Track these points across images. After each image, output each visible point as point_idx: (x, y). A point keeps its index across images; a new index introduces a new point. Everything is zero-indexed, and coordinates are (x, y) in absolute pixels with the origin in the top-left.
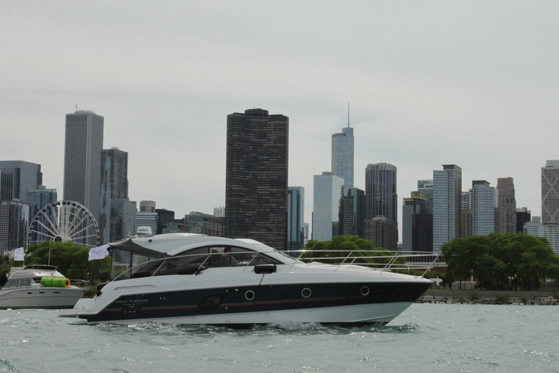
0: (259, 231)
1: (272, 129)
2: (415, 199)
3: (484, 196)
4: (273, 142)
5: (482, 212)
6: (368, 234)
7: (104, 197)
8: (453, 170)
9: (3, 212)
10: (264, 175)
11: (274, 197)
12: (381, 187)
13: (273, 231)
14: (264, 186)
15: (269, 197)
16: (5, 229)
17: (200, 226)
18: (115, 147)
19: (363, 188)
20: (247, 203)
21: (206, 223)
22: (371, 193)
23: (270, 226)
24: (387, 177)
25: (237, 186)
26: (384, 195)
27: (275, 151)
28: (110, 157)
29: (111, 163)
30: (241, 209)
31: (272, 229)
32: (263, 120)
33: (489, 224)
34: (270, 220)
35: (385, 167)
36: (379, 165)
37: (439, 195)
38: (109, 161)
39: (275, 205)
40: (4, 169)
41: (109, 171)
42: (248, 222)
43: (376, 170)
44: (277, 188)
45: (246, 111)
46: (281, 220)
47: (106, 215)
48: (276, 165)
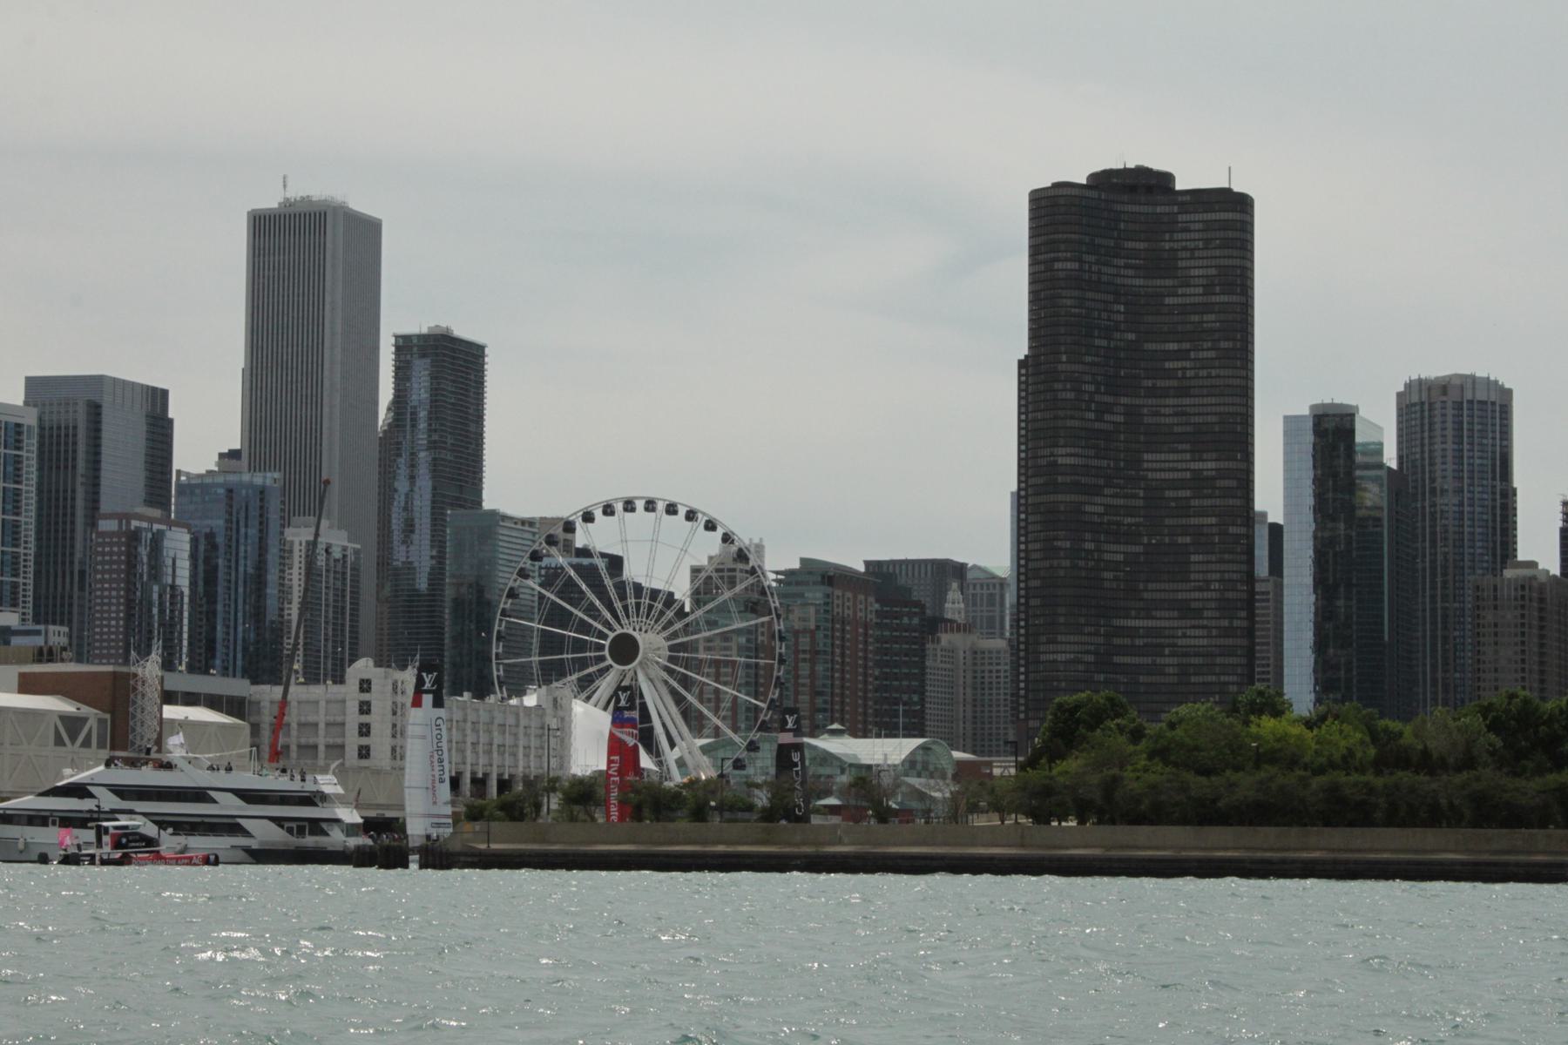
0: (1153, 618)
4: (1201, 290)
7: (407, 503)
9: (111, 556)
10: (1167, 411)
11: (1210, 491)
12: (1459, 458)
13: (1207, 618)
14: (1169, 452)
15: (1188, 493)
16: (110, 619)
17: (812, 604)
18: (444, 325)
19: (1394, 465)
23: (1195, 600)
24: (1480, 427)
25: (1072, 450)
26: (1469, 492)
27: (1207, 322)
28: (428, 361)
29: (432, 384)
30: (1088, 536)
31: (1203, 609)
32: (1159, 209)
35: (1474, 388)
38: (424, 375)
39: (1213, 520)
40: (44, 405)
42: (1114, 585)
43: (1444, 399)
45: (1093, 177)
46: (1235, 576)
47: (414, 568)
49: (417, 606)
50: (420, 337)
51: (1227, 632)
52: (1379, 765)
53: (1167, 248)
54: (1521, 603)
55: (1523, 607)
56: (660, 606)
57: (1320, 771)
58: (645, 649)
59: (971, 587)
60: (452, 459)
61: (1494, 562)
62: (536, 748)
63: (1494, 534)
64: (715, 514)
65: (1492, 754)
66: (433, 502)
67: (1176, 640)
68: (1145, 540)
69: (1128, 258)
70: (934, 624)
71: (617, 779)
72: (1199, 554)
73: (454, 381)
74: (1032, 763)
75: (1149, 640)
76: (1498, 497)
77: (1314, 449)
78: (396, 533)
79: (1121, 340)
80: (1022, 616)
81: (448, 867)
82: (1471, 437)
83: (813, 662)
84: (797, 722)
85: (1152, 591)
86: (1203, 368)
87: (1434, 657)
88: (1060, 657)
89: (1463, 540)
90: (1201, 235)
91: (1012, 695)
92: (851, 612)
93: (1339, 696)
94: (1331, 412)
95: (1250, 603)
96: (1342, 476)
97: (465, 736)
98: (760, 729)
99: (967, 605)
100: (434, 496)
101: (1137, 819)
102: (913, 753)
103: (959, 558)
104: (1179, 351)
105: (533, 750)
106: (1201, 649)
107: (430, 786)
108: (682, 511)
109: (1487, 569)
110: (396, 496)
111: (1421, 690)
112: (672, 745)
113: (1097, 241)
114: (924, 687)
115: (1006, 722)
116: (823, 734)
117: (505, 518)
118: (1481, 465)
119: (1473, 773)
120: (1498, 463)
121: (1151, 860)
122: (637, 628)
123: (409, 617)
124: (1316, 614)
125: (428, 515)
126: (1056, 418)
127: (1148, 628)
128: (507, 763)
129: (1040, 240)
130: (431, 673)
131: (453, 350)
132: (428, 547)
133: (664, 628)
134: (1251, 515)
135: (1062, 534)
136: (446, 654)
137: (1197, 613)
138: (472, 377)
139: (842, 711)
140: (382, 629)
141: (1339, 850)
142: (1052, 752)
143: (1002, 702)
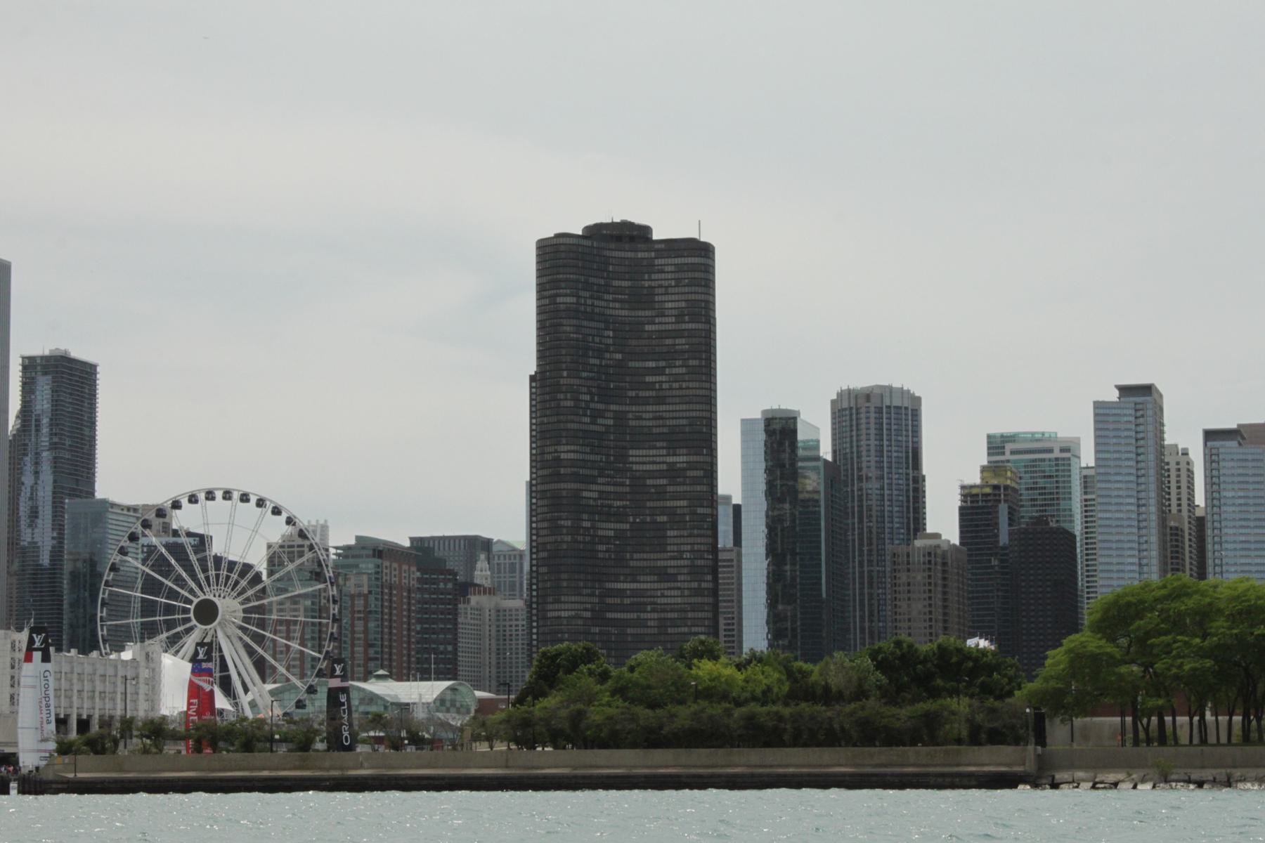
1: (670, 282)
2: (996, 487)
3: (1240, 475)
4: (673, 319)
5: (1234, 519)
6: (906, 588)
7: (32, 494)
8: (1148, 398)
11: (681, 480)
12: (880, 452)
13: (681, 581)
14: (650, 448)
15: (664, 481)
17: (364, 573)
18: (62, 348)
19: (829, 458)
20: (603, 499)
21: (382, 564)
22: (849, 466)
23: (671, 567)
24: (896, 427)
25: (573, 448)
26: (888, 478)
27: (678, 345)
28: (49, 377)
29: (52, 396)
30: (585, 516)
32: (640, 255)
33: (1253, 554)
34: (669, 548)
35: (891, 396)
36: (872, 392)
37: (1109, 470)
39: (684, 503)
41: (48, 420)
43: (867, 405)
44: (690, 455)
45: (587, 229)
46: (702, 548)
47: (38, 547)
48: (684, 386)
49: (41, 578)
50: (42, 358)
51: (697, 592)
52: (792, 697)
53: (647, 285)
54: (927, 566)
55: (930, 569)
56: (236, 577)
57: (738, 704)
58: (223, 612)
59: (496, 558)
60: (70, 457)
61: (908, 534)
62: (131, 694)
63: (908, 512)
64: (280, 502)
65: (879, 688)
66: (54, 493)
67: (655, 599)
68: (631, 519)
69: (615, 294)
70: (466, 588)
71: (196, 718)
72: (673, 529)
73: (71, 394)
74: (520, 701)
75: (635, 599)
76: (911, 483)
77: (765, 445)
78: (23, 518)
79: (610, 359)
80: (534, 581)
81: (42, 793)
82: (889, 435)
83: (366, 620)
84: (343, 669)
85: (637, 560)
86: (676, 382)
87: (862, 610)
88: (563, 614)
89: (884, 517)
90: (673, 276)
91: (528, 644)
92: (397, 579)
93: (786, 642)
94: (778, 416)
95: (714, 571)
96: (787, 466)
97: (72, 684)
98: (317, 675)
99: (493, 573)
100: (54, 487)
101: (604, 745)
102: (443, 693)
103: (485, 534)
104: (657, 368)
105: (63, 691)
106: (676, 606)
107: (39, 726)
108: (253, 499)
109: (903, 539)
110: (23, 488)
111: (852, 636)
112: (246, 690)
113: (592, 280)
114: (456, 639)
115: (522, 667)
116: (371, 678)
117: (113, 505)
118: (898, 457)
119: (859, 704)
120: (910, 454)
121: (608, 777)
122: (217, 595)
123: (34, 587)
124: (768, 577)
125: (50, 503)
126: (559, 422)
127: (633, 590)
128: (63, 705)
129: (545, 280)
130: (40, 634)
131: (71, 369)
132: (50, 530)
133: (239, 595)
134: (715, 498)
135: (564, 515)
136: (65, 617)
137: (672, 578)
138: (87, 391)
139: (390, 660)
140: (12, 597)
141: (756, 766)
142: (534, 692)
143: (520, 651)
